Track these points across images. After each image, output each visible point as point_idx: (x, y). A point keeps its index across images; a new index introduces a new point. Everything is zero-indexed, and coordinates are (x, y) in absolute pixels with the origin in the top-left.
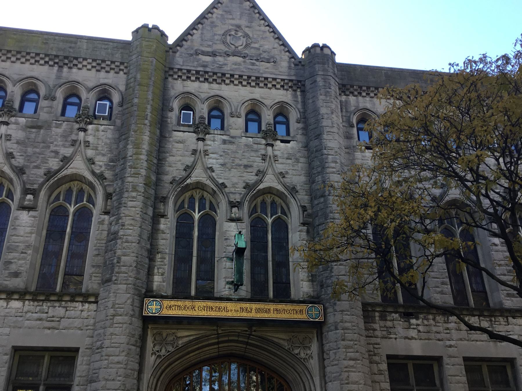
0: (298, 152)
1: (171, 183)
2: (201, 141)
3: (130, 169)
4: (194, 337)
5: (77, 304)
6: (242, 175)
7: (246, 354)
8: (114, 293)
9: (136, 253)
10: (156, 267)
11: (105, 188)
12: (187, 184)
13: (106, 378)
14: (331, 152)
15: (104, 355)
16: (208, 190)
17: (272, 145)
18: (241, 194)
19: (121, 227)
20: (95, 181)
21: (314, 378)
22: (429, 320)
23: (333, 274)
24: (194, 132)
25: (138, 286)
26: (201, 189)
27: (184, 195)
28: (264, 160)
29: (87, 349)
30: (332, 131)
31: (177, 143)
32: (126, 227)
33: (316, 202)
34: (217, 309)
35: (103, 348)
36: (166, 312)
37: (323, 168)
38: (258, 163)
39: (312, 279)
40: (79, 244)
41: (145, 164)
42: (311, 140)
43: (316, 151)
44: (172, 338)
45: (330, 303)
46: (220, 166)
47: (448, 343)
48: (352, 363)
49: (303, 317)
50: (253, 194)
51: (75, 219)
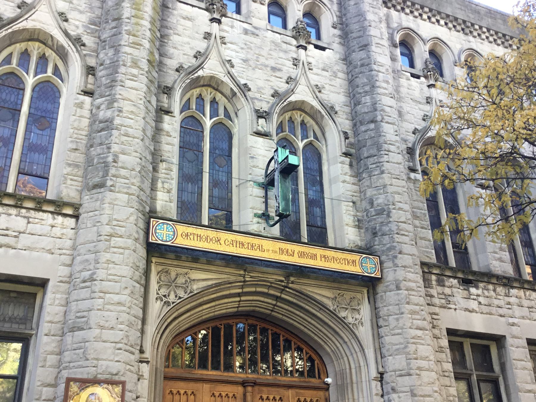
0: (336, 64)
1: (177, 70)
2: (216, 22)
3: (128, 36)
4: (214, 282)
5: (45, 216)
6: (269, 78)
7: (274, 314)
8: (109, 203)
9: (140, 154)
10: (159, 180)
11: (83, 57)
12: (198, 77)
13: (101, 324)
14: (381, 69)
15: (97, 290)
16: (224, 91)
17: (305, 48)
18: (268, 102)
19: (118, 113)
20: (69, 46)
21: (366, 350)
22: (490, 291)
23: (391, 220)
24: (207, 10)
25: (142, 200)
26: (214, 88)
27: (191, 92)
28: (296, 66)
29: (61, 282)
30: (381, 43)
31: (184, 18)
32: (125, 115)
33: (363, 128)
34: (250, 247)
35: (95, 280)
36: (181, 242)
37: (373, 87)
38: (289, 69)
39: (359, 224)
40: (41, 132)
41: (148, 34)
42: (354, 51)
43: (362, 65)
44: (184, 281)
45: (387, 256)
46: (241, 61)
47: (511, 320)
48: (419, 333)
49: (356, 269)
50: (283, 105)
51: (35, 96)
